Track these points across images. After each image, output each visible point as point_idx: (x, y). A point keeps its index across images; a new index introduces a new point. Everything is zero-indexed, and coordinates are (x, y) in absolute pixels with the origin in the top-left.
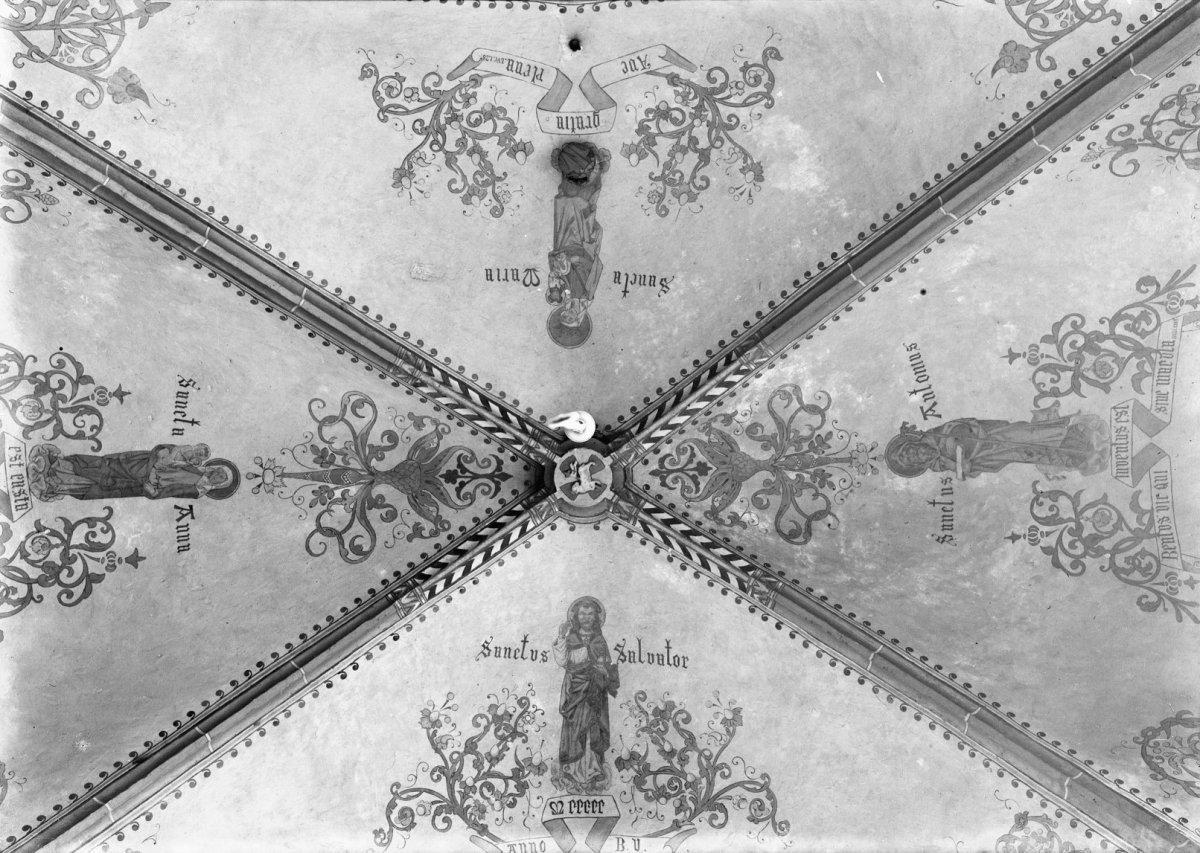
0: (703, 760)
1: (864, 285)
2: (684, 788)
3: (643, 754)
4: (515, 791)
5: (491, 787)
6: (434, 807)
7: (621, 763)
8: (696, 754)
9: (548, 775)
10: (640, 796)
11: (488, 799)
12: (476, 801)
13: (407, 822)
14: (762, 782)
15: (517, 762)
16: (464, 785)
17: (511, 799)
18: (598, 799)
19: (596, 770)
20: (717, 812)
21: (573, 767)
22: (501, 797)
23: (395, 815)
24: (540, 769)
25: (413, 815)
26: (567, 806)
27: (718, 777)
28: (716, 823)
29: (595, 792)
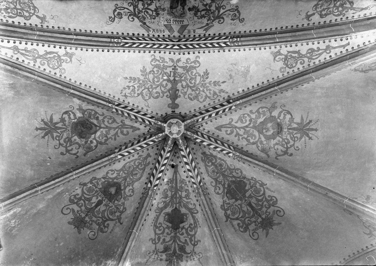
0: (217, 5)
1: (354, 31)
2: (210, 14)
3: (197, 6)
4: (155, 15)
5: (147, 12)
6: (129, 14)
7: (190, 9)
8: (215, 4)
9: (166, 12)
10: (196, 18)
11: (147, 15)
12: (142, 15)
13: (120, 16)
14: (236, 8)
15: (156, 7)
16: (139, 10)
17: (154, 17)
18: (182, 20)
19: (182, 12)
20: (221, 19)
21: (174, 10)
22: (150, 16)
23: (116, 13)
24: (164, 10)
25: (122, 15)
26: (172, 21)
27: (221, 9)
28: (220, 22)
29: (181, 18)
